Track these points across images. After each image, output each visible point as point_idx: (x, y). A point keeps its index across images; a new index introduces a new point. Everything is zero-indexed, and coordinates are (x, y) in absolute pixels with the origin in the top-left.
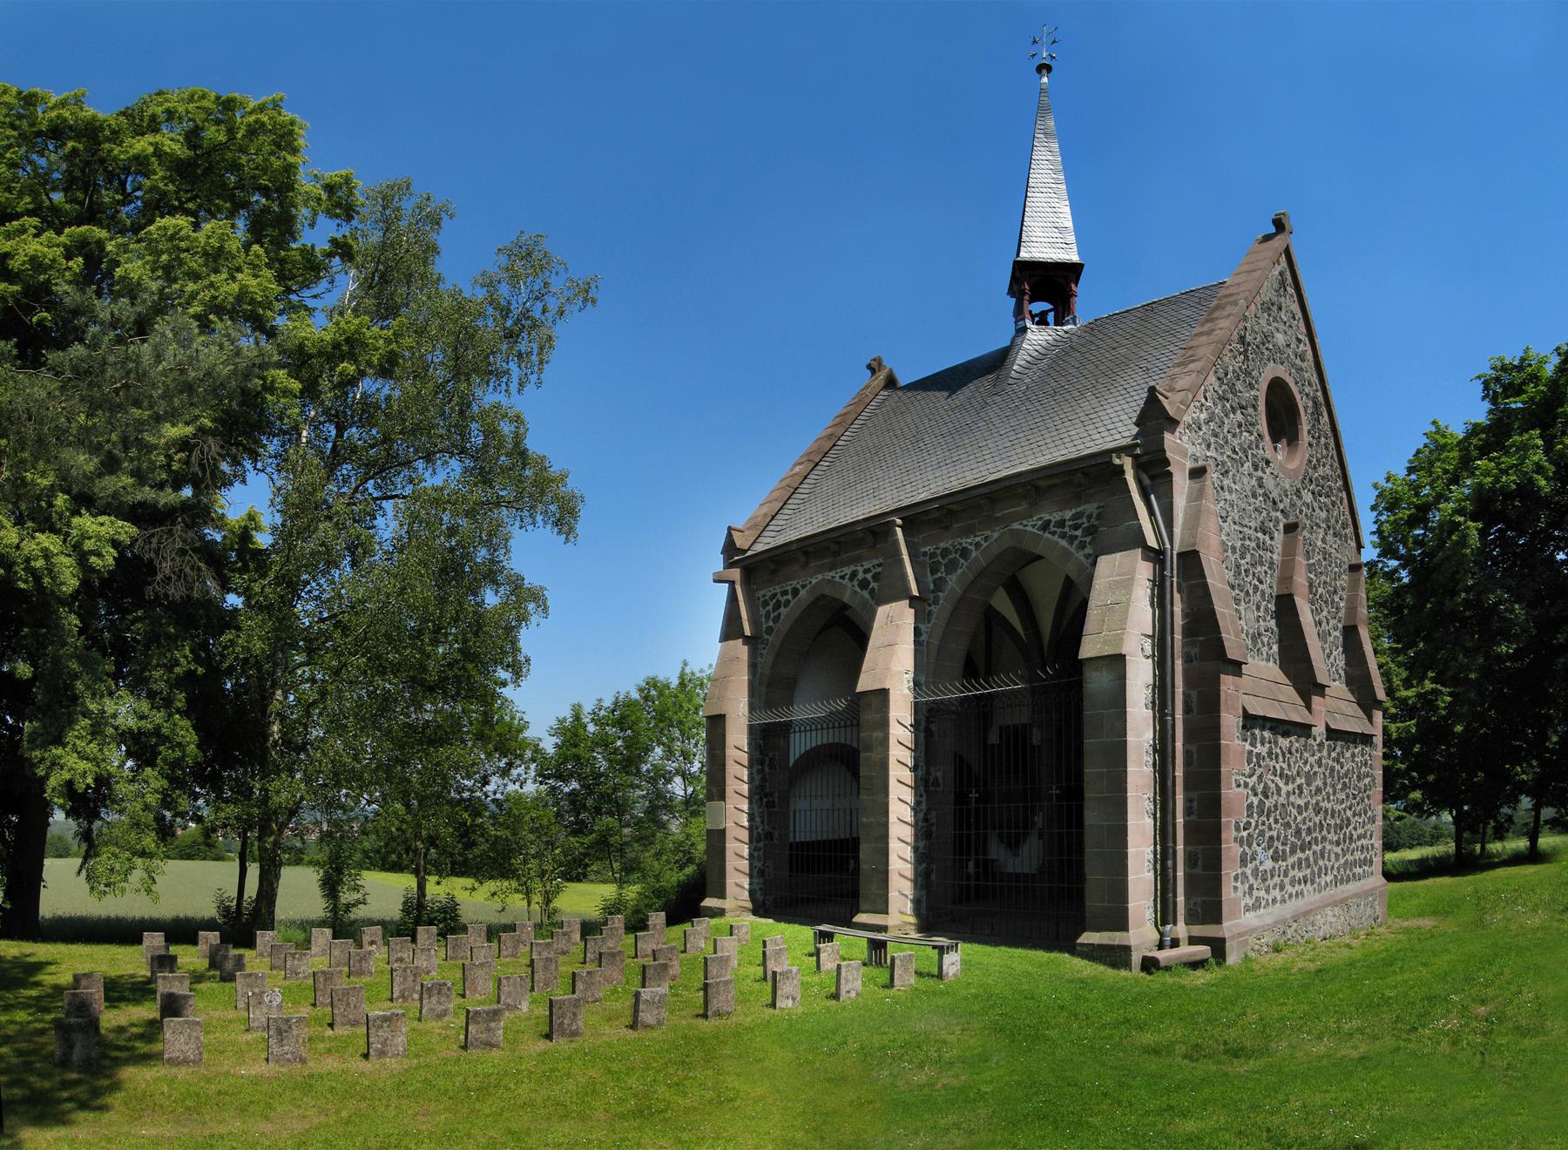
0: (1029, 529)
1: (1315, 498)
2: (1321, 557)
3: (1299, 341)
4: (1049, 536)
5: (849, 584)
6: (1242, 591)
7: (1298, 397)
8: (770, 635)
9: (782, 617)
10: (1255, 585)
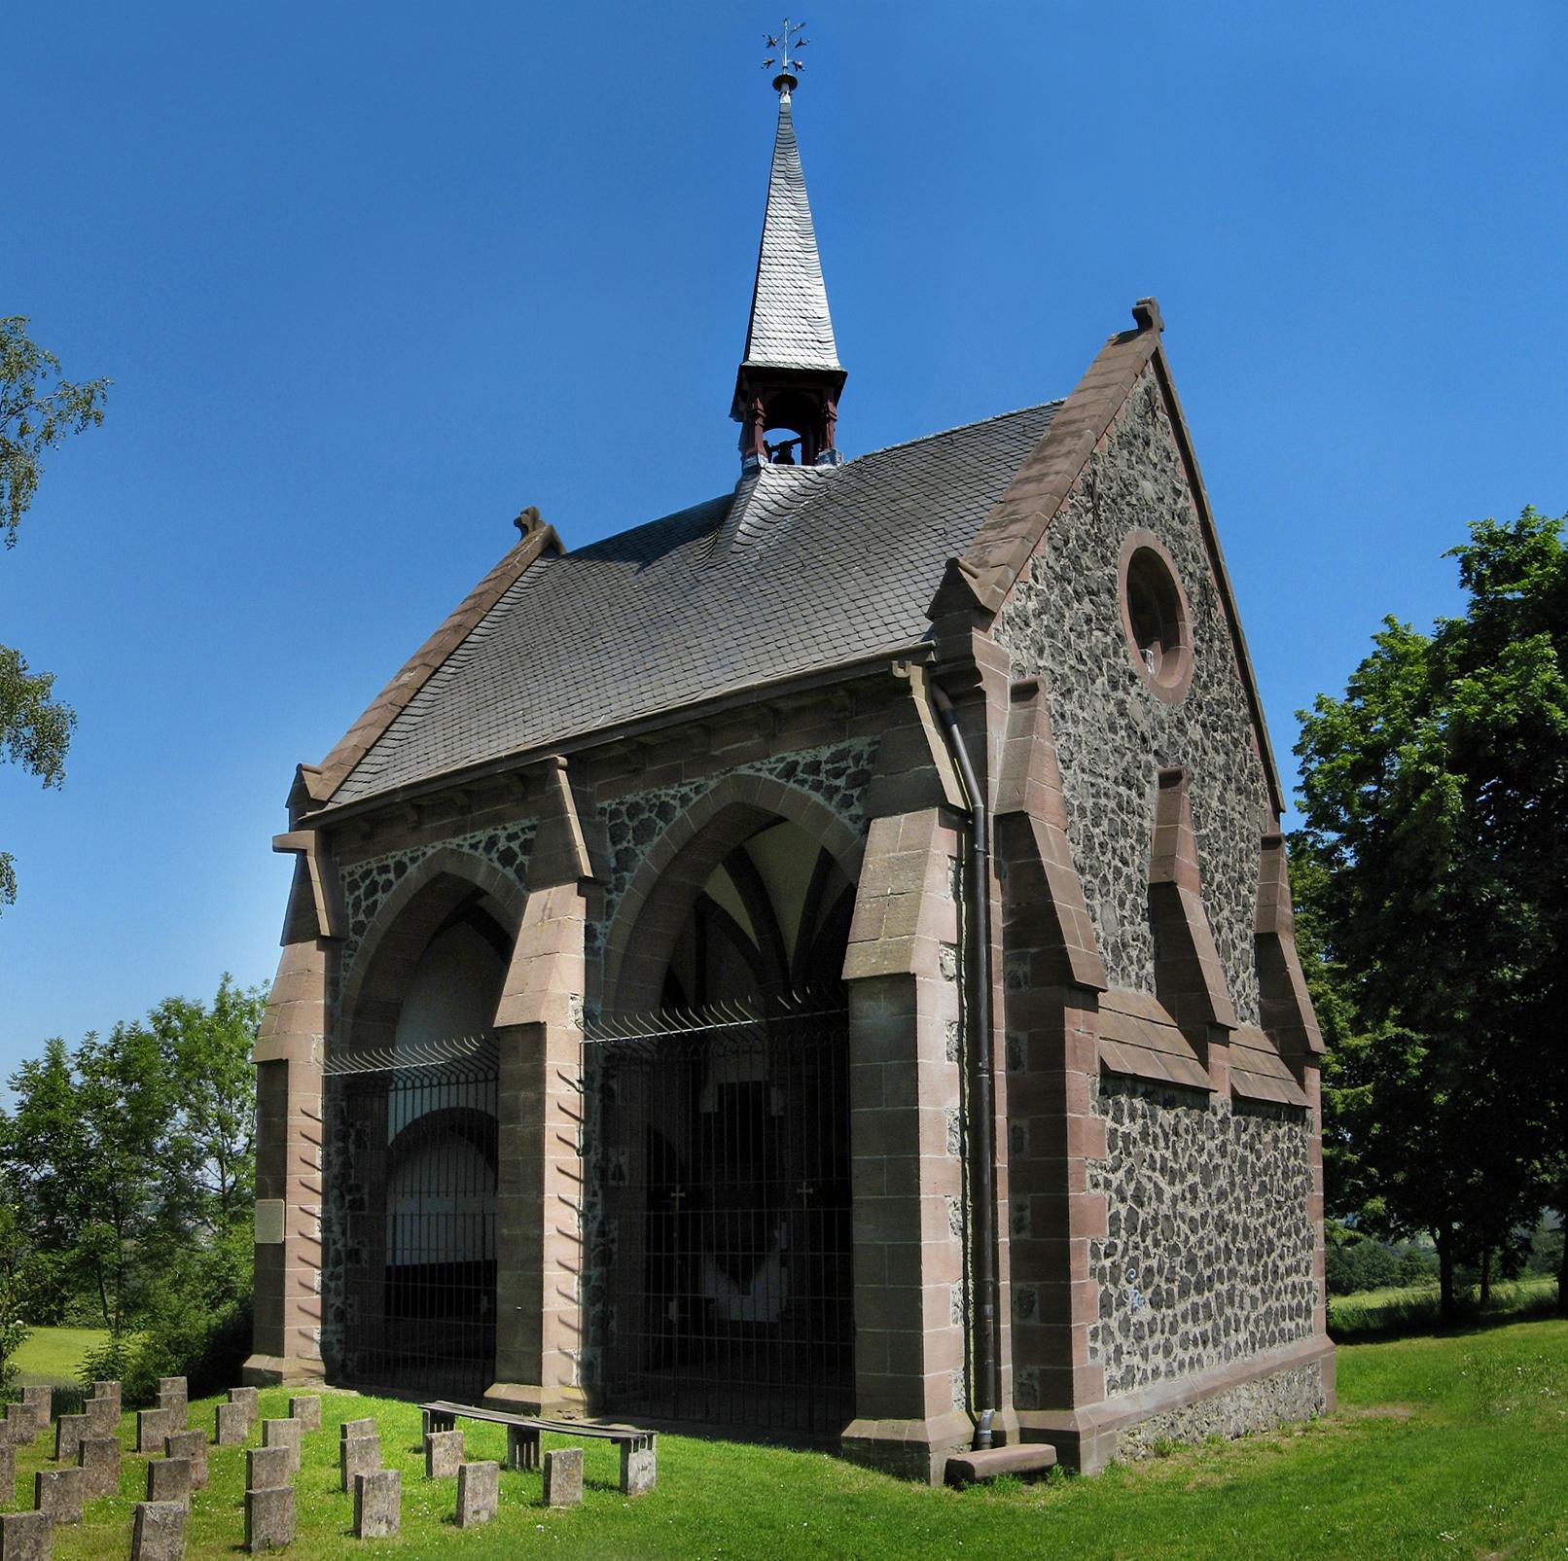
0: (765, 775)
1: (1206, 734)
2: (1217, 825)
5: (484, 858)
9: (380, 907)
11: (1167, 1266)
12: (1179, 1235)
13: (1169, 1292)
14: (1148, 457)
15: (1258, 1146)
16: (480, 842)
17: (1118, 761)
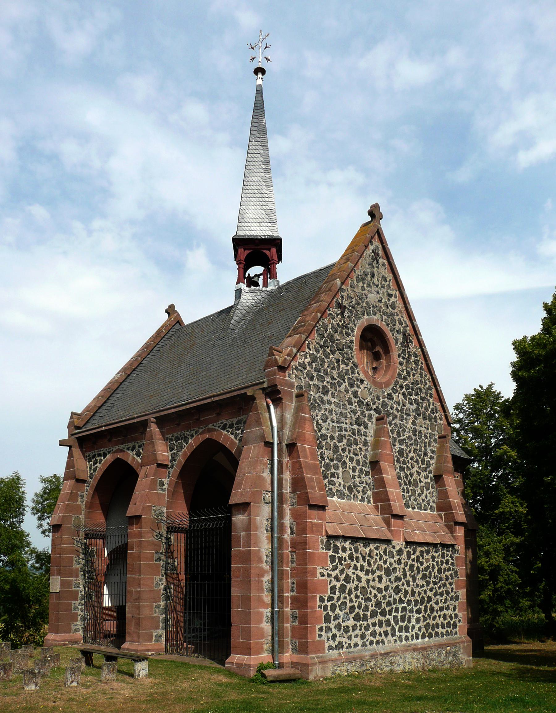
7: (389, 335)
14: (373, 283)
15: (421, 560)
16: (130, 447)
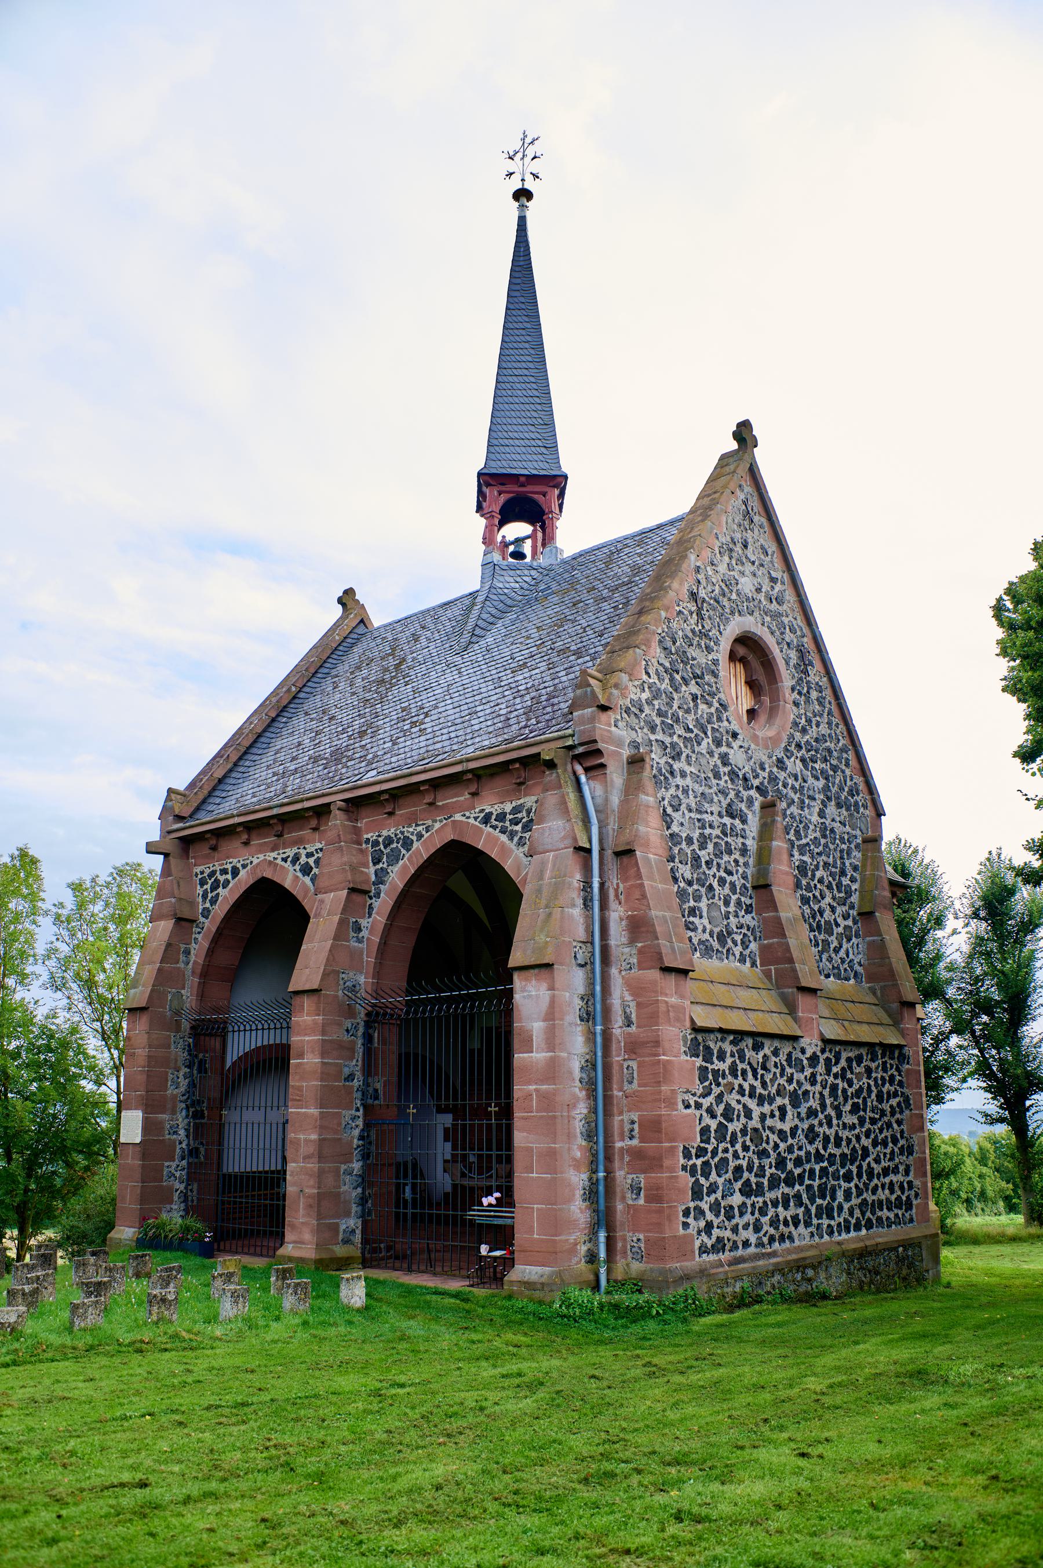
0: (472, 821)
1: (806, 767)
2: (818, 834)
3: (773, 580)
4: (491, 830)
5: (291, 868)
6: (703, 886)
8: (207, 918)
9: (220, 898)
10: (721, 878)
11: (756, 1165)
12: (768, 1143)
13: (759, 1185)
15: (849, 1076)
17: (722, 799)
